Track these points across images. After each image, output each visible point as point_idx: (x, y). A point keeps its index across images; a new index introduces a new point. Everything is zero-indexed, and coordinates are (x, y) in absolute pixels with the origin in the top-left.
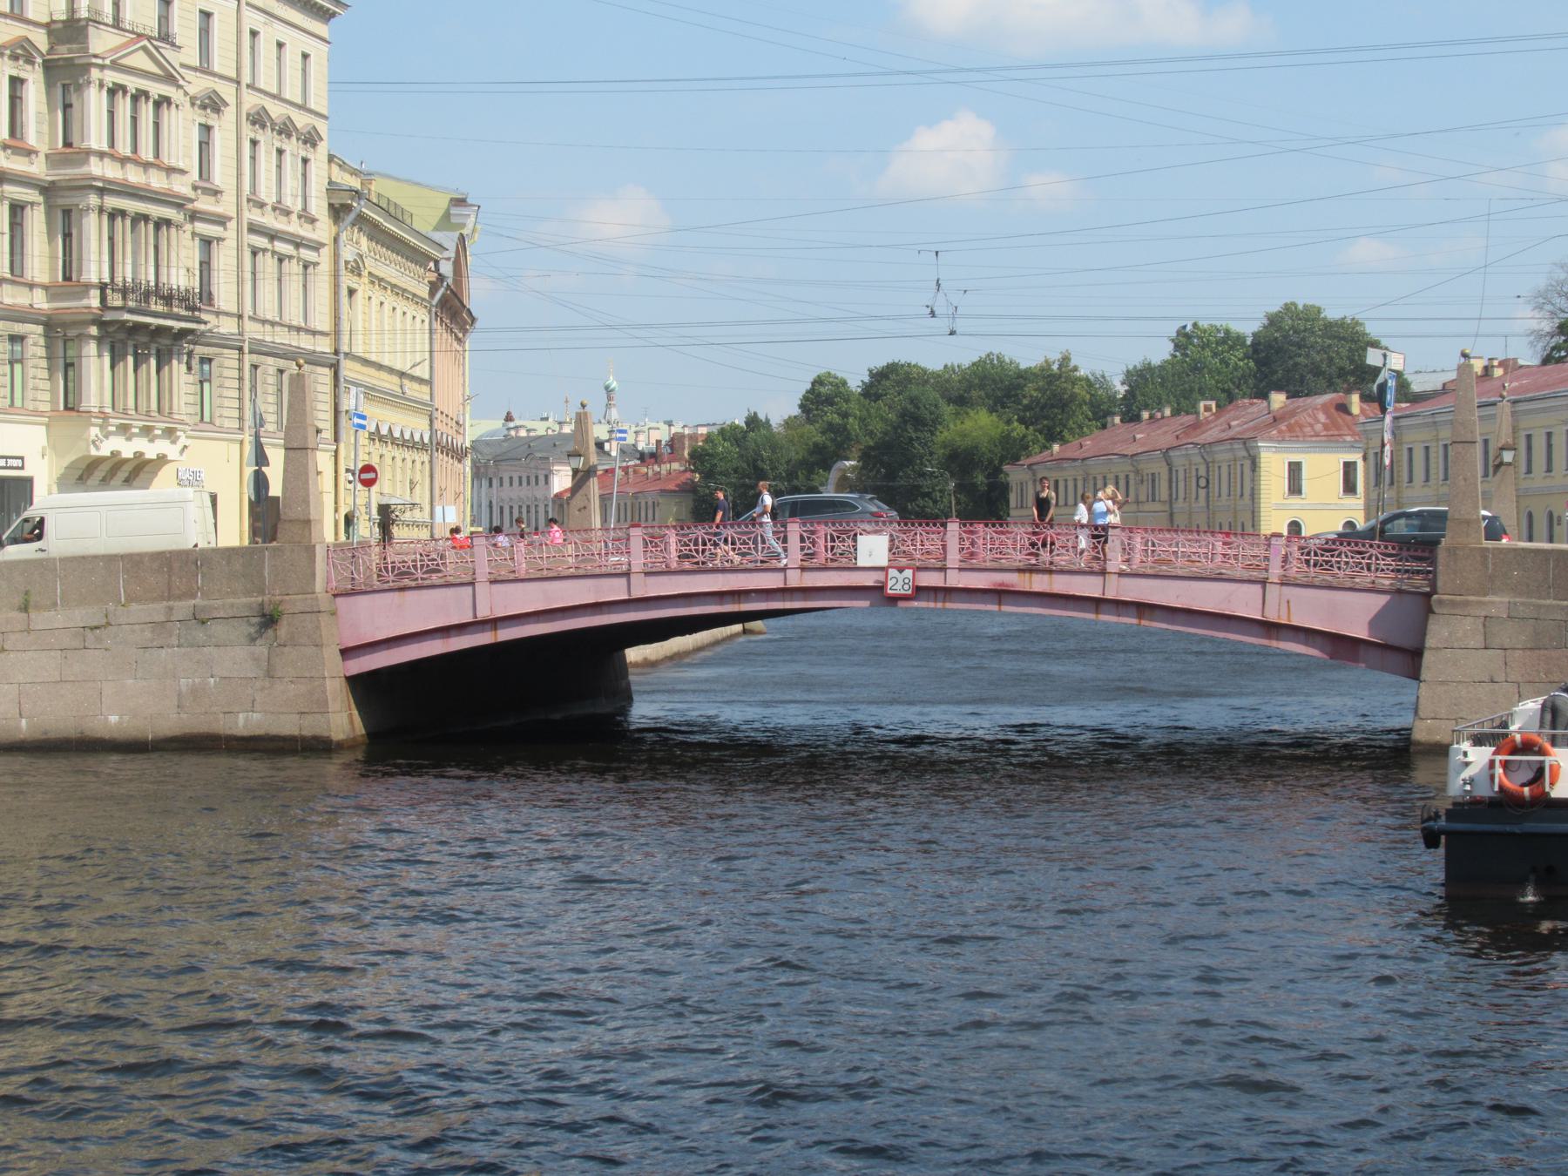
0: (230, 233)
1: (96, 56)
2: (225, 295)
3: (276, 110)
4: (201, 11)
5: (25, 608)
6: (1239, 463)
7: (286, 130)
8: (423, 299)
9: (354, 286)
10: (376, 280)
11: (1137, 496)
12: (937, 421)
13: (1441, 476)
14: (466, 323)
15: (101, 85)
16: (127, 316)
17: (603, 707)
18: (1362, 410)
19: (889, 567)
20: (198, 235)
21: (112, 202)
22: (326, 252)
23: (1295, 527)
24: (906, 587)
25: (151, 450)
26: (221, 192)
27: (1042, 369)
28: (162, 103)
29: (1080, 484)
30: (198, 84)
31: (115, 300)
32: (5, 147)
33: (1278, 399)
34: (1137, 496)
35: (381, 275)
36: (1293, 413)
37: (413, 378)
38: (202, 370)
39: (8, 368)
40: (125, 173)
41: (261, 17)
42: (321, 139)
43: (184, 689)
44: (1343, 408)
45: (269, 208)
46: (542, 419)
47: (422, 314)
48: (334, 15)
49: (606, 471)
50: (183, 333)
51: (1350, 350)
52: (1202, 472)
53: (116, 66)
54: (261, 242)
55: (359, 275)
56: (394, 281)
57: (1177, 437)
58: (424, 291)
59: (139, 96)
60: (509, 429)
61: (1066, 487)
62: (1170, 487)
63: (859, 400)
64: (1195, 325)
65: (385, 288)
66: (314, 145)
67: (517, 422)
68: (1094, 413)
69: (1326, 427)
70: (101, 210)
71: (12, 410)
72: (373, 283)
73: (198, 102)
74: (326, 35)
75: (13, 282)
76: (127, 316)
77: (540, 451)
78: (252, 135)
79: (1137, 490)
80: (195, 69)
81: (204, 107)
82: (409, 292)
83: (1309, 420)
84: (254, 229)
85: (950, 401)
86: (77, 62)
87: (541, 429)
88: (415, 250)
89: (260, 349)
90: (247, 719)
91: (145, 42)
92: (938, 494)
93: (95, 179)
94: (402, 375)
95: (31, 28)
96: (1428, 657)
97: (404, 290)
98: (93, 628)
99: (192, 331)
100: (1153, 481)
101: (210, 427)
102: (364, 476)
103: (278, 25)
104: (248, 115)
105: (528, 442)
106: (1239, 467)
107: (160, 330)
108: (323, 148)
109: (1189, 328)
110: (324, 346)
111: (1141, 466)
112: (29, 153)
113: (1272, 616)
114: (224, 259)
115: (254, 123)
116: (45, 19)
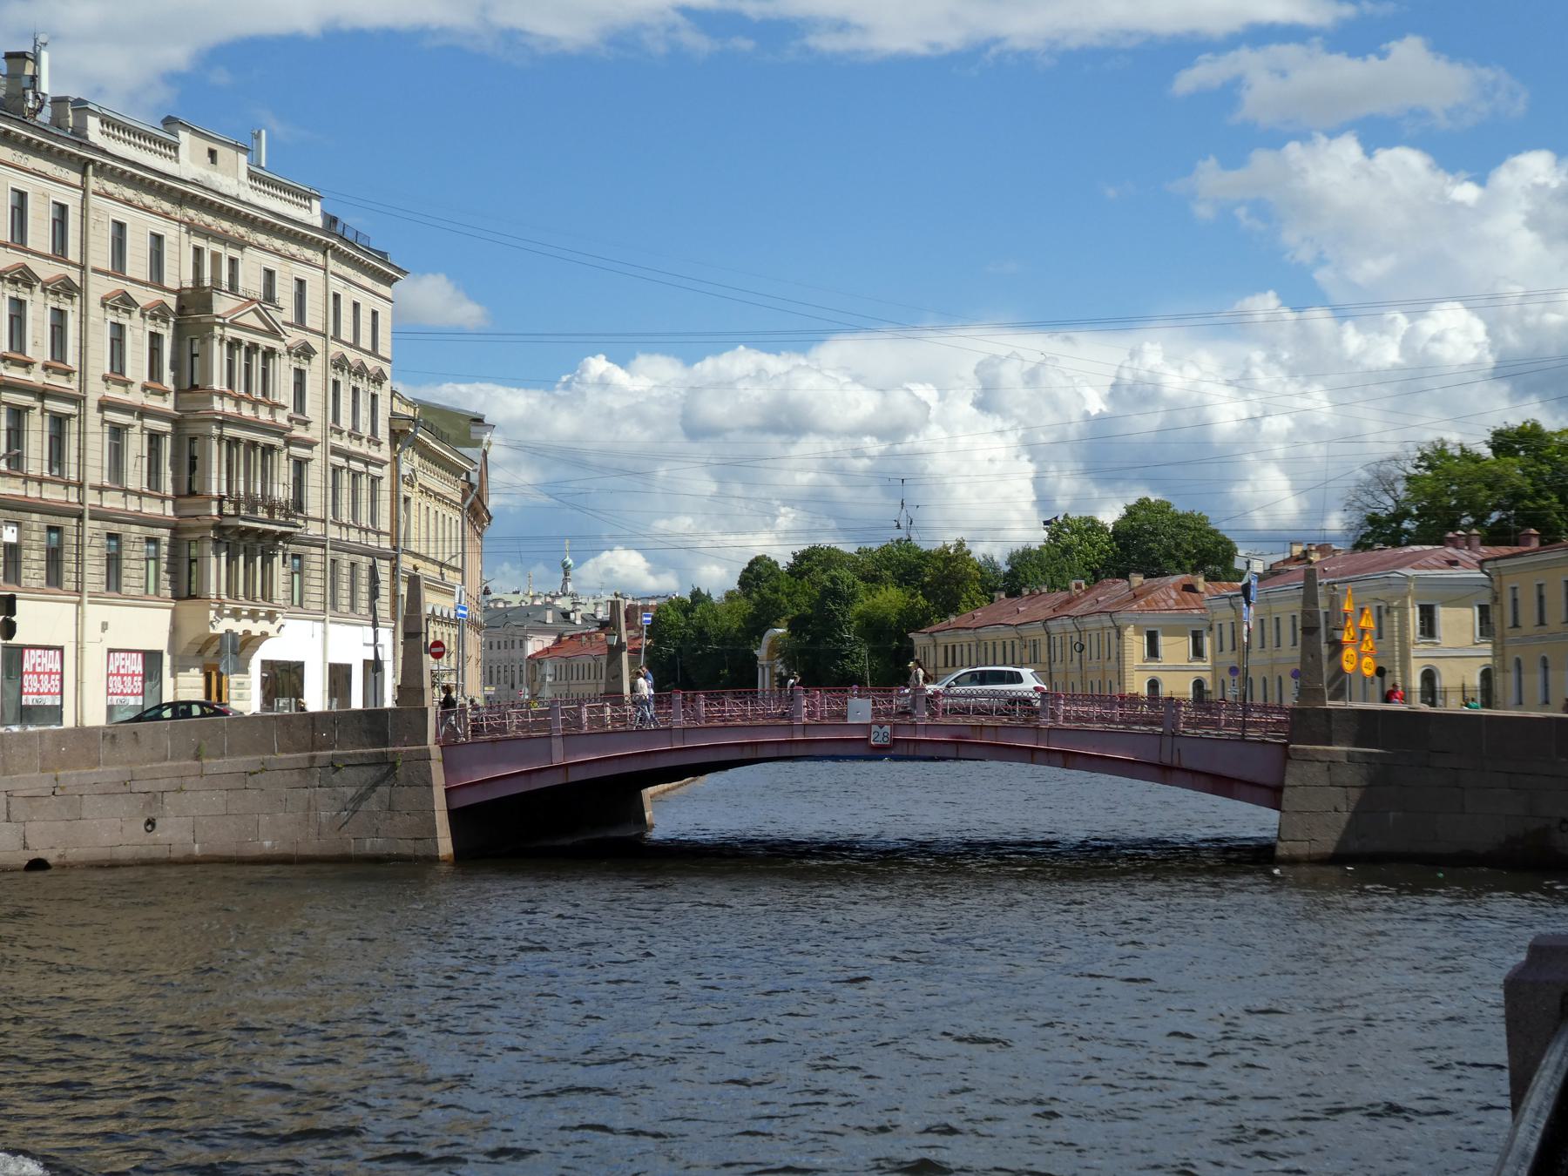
0: (317, 454)
1: (218, 317)
2: (315, 502)
3: (352, 356)
4: (265, 269)
5: (197, 757)
6: (1106, 631)
7: (360, 371)
8: (457, 504)
9: (409, 495)
10: (425, 491)
11: (1021, 659)
12: (853, 596)
13: (1274, 644)
14: (483, 521)
15: (222, 340)
16: (241, 523)
17: (633, 832)
18: (1206, 588)
19: (872, 724)
20: (107, 422)
21: (229, 432)
22: (387, 468)
23: (1153, 685)
24: (886, 739)
25: (256, 628)
26: (310, 422)
27: (941, 552)
28: (270, 353)
29: (973, 649)
30: (295, 337)
31: (229, 509)
32: (4, 359)
33: (1137, 580)
34: (1021, 659)
35: (428, 485)
36: (1150, 591)
37: (450, 568)
38: (293, 564)
39: (144, 563)
40: (256, 412)
41: (341, 283)
42: (386, 379)
43: (324, 820)
44: (1190, 588)
45: (346, 434)
46: (514, 593)
47: (457, 516)
48: (397, 279)
49: (572, 637)
50: (283, 536)
51: (1194, 537)
52: (1076, 639)
53: (234, 325)
54: (340, 461)
55: (413, 486)
56: (437, 490)
57: (1054, 610)
58: (458, 498)
59: (252, 349)
60: (488, 602)
61: (970, 650)
62: (1049, 652)
63: (787, 579)
64: (1066, 516)
65: (431, 496)
66: (380, 384)
67: (494, 595)
68: (983, 588)
69: (1177, 603)
70: (221, 438)
71: (147, 597)
72: (422, 492)
73: (148, 313)
74: (390, 296)
75: (150, 496)
76: (241, 523)
77: (516, 620)
78: (334, 376)
79: (1021, 653)
80: (291, 325)
81: (153, 317)
82: (448, 499)
83: (1163, 596)
84: (336, 451)
85: (863, 579)
86: (203, 321)
87: (515, 602)
88: (453, 464)
89: (338, 546)
90: (372, 843)
91: (256, 305)
92: (855, 656)
93: (217, 414)
94: (442, 565)
95: (166, 294)
96: (1287, 793)
97: (444, 497)
98: (251, 774)
99: (290, 534)
100: (1035, 646)
101: (300, 609)
102: (440, 649)
103: (354, 289)
104: (332, 360)
105: (505, 612)
106: (1106, 635)
107: (266, 533)
108: (387, 385)
109: (1060, 519)
110: (386, 544)
111: (1024, 634)
112: (27, 365)
113: (1166, 760)
114: (315, 477)
115: (335, 368)
116: (176, 287)
